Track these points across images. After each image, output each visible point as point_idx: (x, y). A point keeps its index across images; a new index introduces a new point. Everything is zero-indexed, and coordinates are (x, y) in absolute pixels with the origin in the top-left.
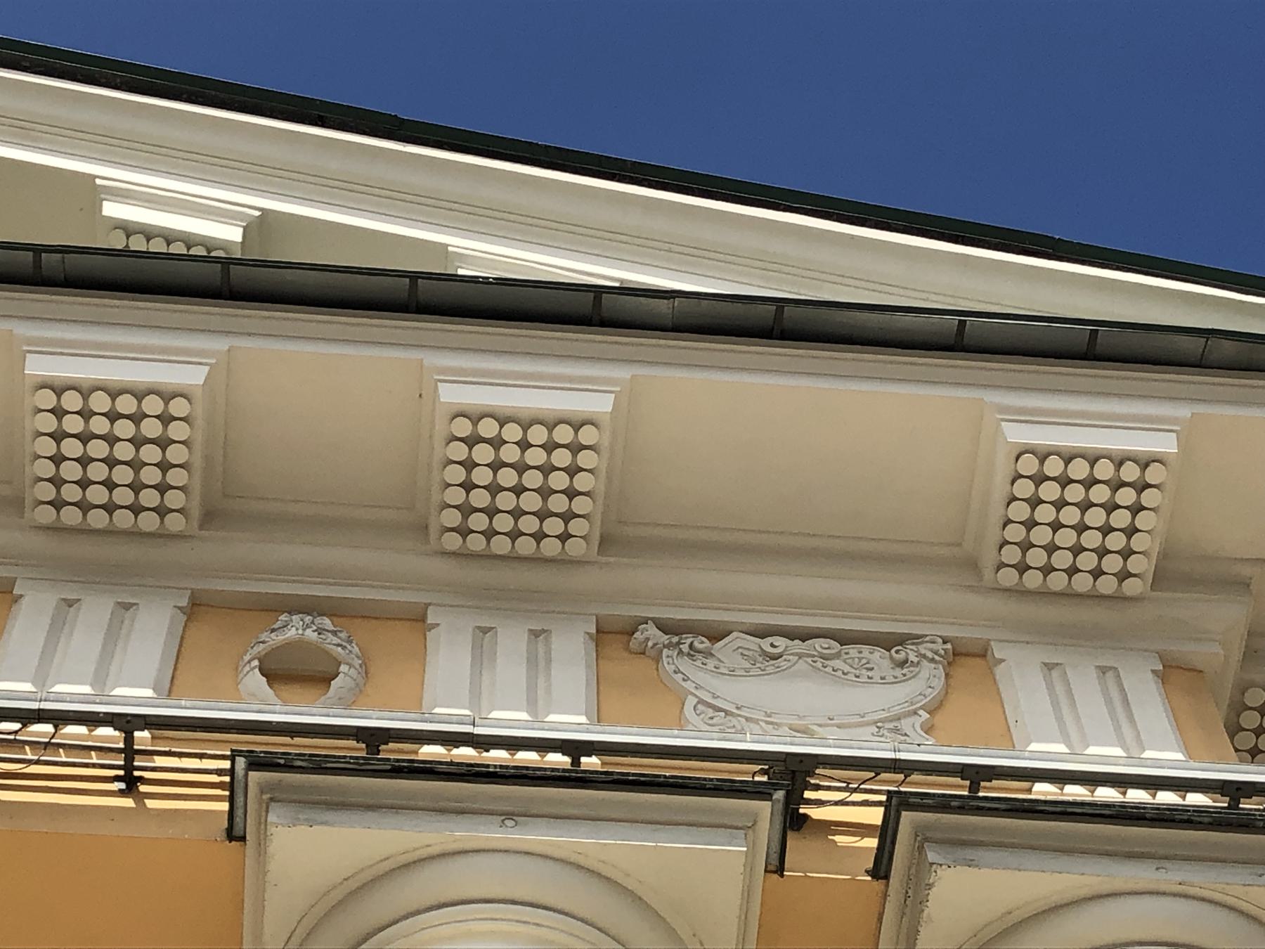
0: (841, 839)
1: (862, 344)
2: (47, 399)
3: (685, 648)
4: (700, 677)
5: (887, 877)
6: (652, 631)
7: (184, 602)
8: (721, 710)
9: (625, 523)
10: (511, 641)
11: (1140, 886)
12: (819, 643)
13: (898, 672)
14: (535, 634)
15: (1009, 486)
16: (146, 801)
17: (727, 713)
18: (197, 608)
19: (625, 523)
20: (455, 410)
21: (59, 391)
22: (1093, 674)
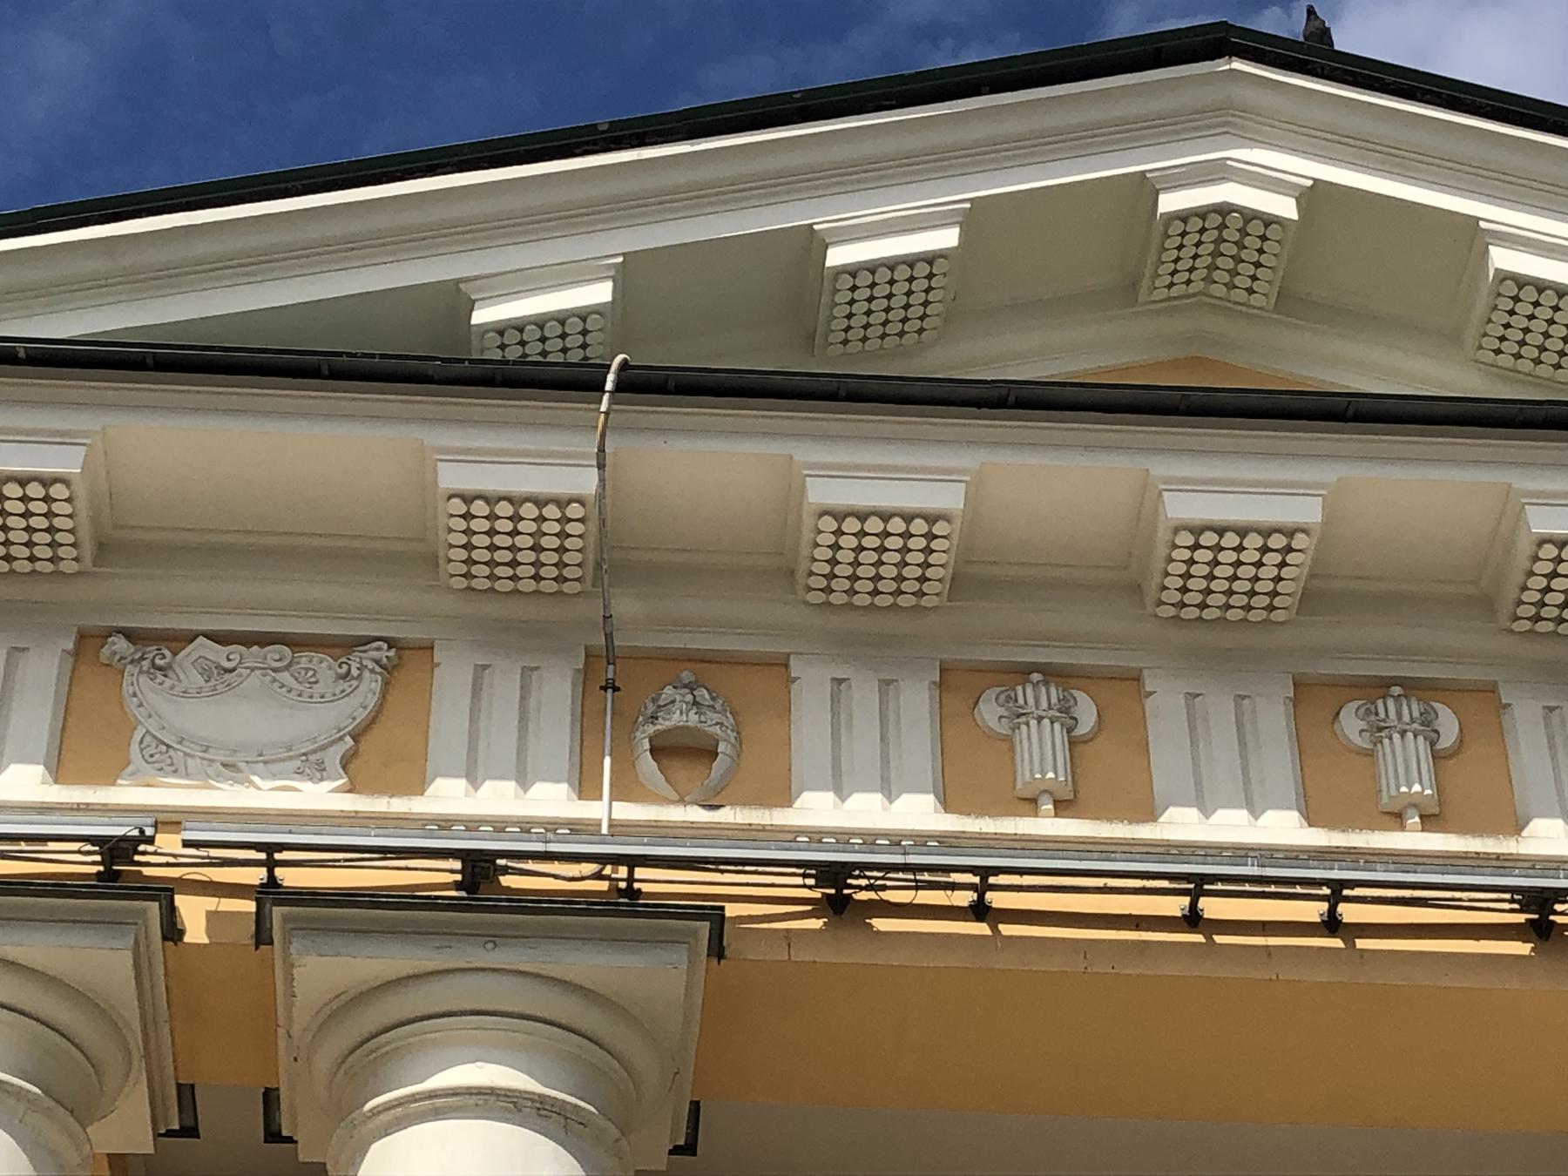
0: (881, 924)
1: (979, 406)
2: (458, 506)
3: (146, 664)
4: (151, 697)
6: (120, 644)
7: (70, 646)
8: (163, 743)
9: (122, 527)
10: (1219, 706)
11: (583, 1026)
12: (273, 652)
13: (343, 685)
14: (886, 683)
15: (1534, 548)
16: (501, 878)
17: (168, 746)
18: (1304, 691)
19: (122, 527)
20: (1177, 523)
21: (468, 499)
22: (1540, 712)
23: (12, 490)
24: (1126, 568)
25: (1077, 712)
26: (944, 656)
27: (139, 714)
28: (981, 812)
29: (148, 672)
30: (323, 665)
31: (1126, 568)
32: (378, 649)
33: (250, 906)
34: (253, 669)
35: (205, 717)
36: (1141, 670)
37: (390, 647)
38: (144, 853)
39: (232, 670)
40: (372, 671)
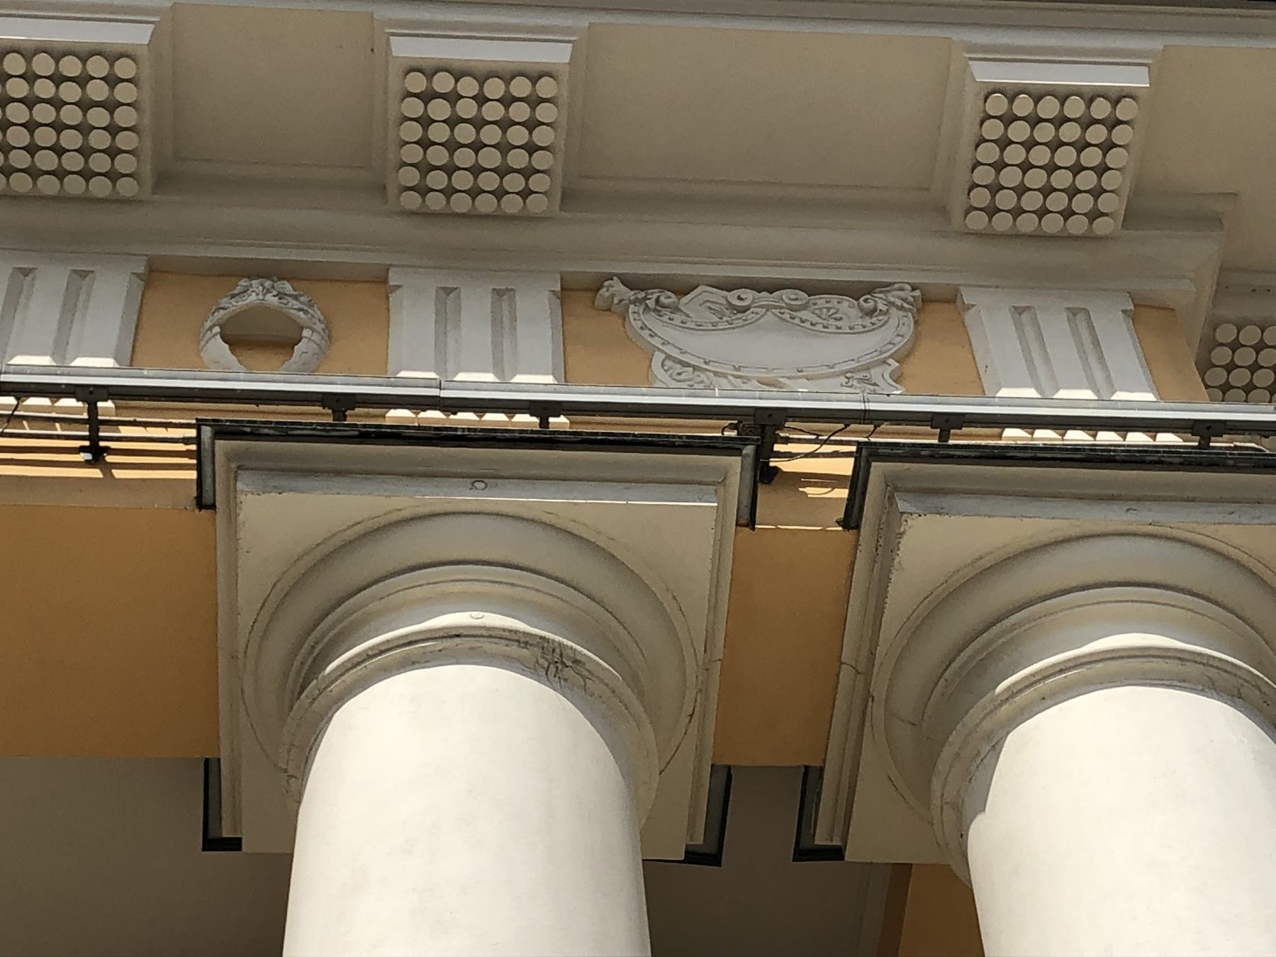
3: (651, 303)
5: (858, 527)
7: (141, 270)
8: (688, 365)
12: (786, 294)
13: (867, 321)
14: (499, 293)
17: (695, 368)
18: (154, 275)
23: (14, 64)
24: (927, 189)
25: (804, 318)
26: (563, 269)
27: (656, 342)
28: (934, 395)
29: (655, 310)
30: (846, 306)
31: (927, 189)
32: (902, 290)
33: (101, 434)
34: (768, 308)
35: (697, 345)
36: (387, 268)
37: (913, 289)
38: (787, 441)
39: (745, 310)
40: (901, 308)
